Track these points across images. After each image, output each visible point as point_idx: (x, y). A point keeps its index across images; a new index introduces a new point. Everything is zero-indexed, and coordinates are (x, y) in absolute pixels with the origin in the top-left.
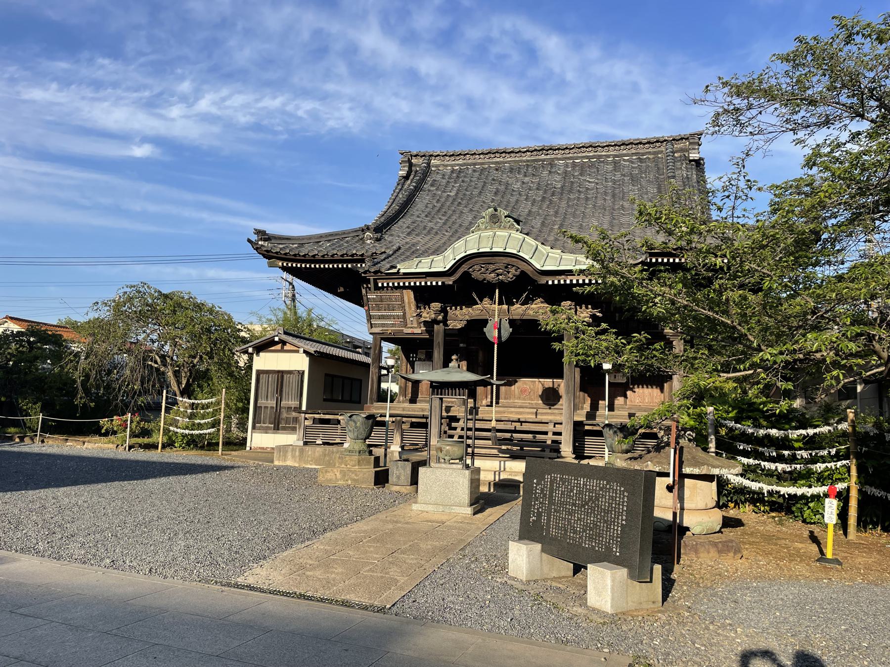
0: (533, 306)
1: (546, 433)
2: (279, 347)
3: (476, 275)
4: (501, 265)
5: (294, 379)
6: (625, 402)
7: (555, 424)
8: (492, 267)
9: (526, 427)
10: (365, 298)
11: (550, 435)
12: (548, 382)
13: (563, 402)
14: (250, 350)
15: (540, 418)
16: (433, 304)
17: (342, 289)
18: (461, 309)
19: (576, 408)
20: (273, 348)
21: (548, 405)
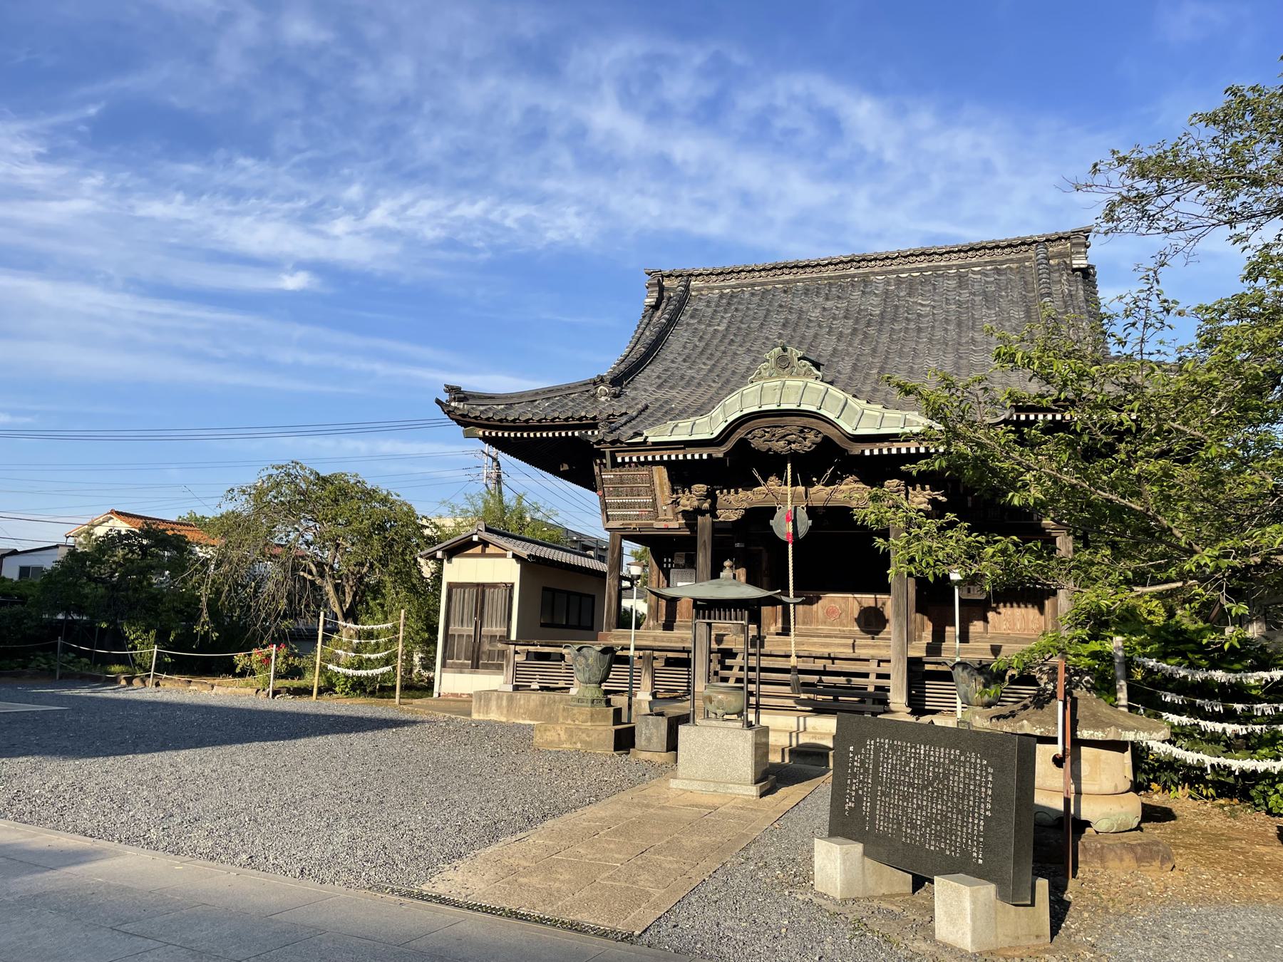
0: (843, 487)
1: (866, 675)
2: (478, 549)
5: (500, 595)
6: (986, 629)
7: (880, 661)
8: (780, 432)
10: (598, 479)
11: (872, 678)
12: (868, 599)
13: (891, 629)
14: (439, 555)
17: (566, 467)
18: (737, 493)
20: (470, 551)
21: (868, 633)
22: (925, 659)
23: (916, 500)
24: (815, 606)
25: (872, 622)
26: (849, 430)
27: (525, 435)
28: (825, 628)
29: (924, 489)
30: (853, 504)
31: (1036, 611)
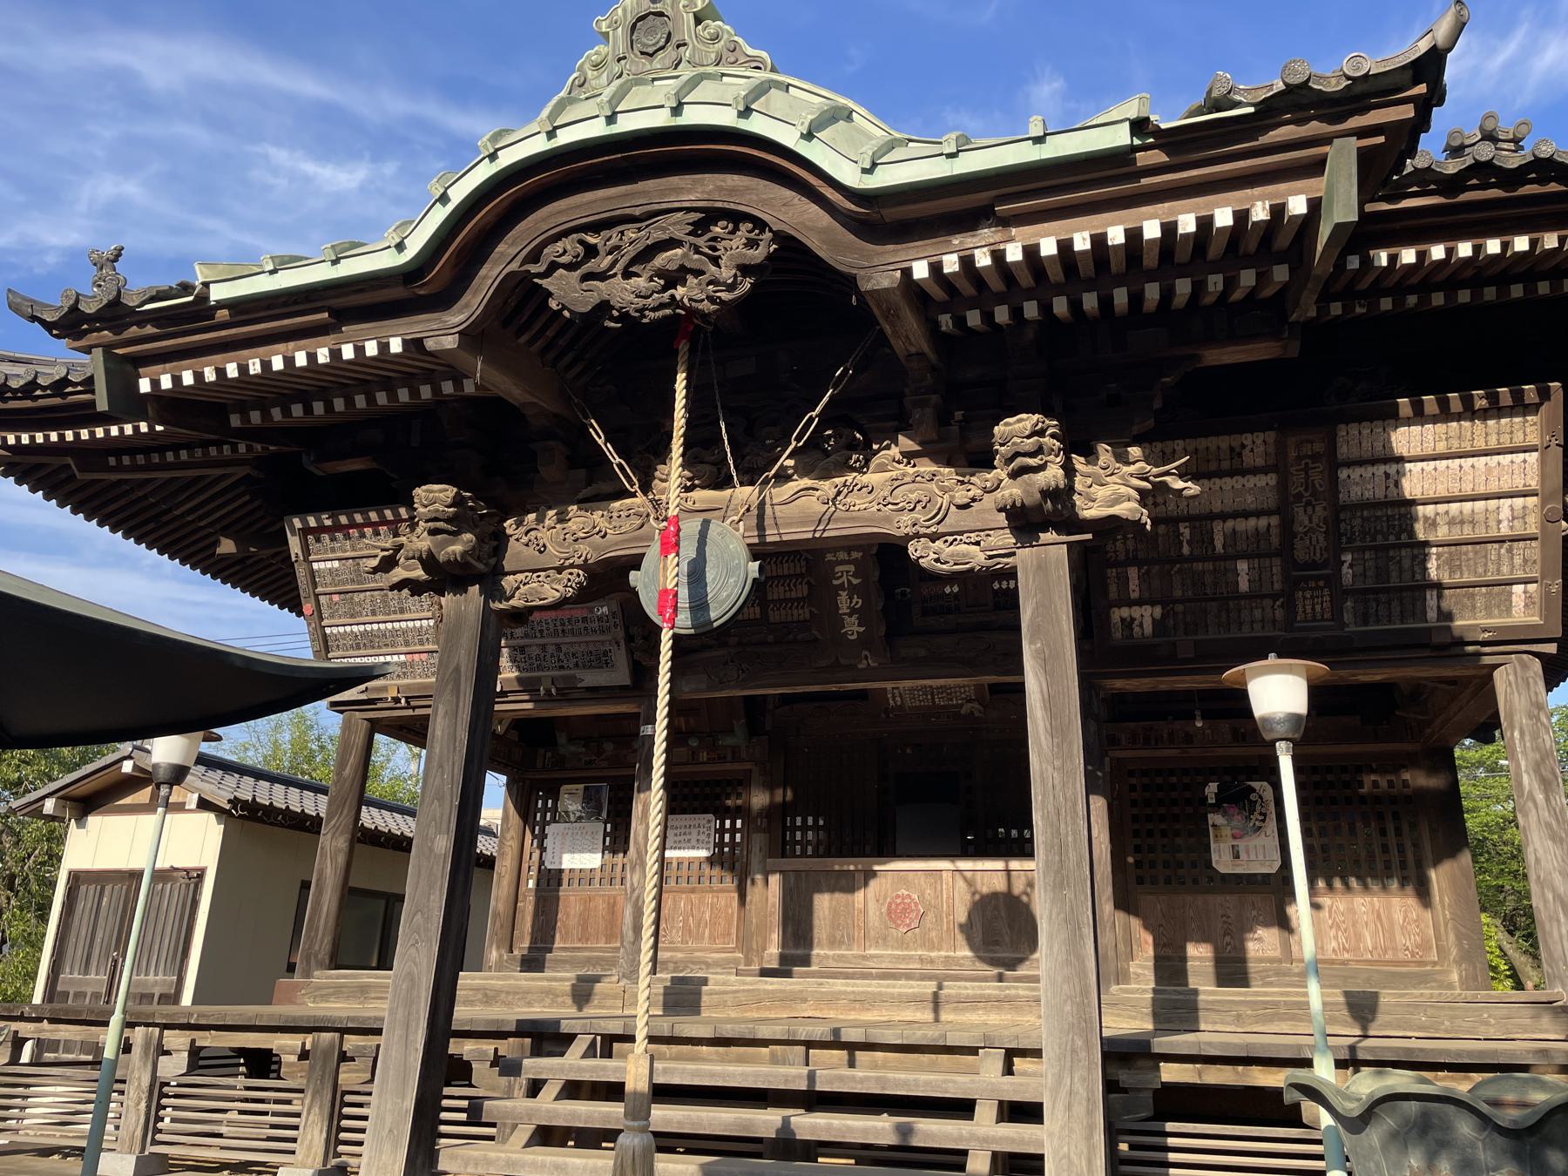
0: (870, 478)
1: (962, 1108)
2: (144, 795)
3: (568, 292)
4: (676, 226)
5: (173, 894)
6: (1287, 947)
7: (1011, 1054)
8: (633, 238)
9: (868, 1076)
10: (301, 572)
11: (986, 1113)
12: (989, 872)
13: (1047, 957)
14: (49, 806)
15: (960, 1024)
16: (420, 492)
17: (227, 546)
18: (562, 519)
19: (1106, 973)
20: (128, 800)
21: (993, 962)
22: (1162, 1044)
23: (1101, 492)
24: (859, 896)
25: (1002, 931)
26: (850, 176)
27: (54, 437)
28: (882, 954)
29: (1123, 459)
30: (901, 525)
31: (1412, 902)
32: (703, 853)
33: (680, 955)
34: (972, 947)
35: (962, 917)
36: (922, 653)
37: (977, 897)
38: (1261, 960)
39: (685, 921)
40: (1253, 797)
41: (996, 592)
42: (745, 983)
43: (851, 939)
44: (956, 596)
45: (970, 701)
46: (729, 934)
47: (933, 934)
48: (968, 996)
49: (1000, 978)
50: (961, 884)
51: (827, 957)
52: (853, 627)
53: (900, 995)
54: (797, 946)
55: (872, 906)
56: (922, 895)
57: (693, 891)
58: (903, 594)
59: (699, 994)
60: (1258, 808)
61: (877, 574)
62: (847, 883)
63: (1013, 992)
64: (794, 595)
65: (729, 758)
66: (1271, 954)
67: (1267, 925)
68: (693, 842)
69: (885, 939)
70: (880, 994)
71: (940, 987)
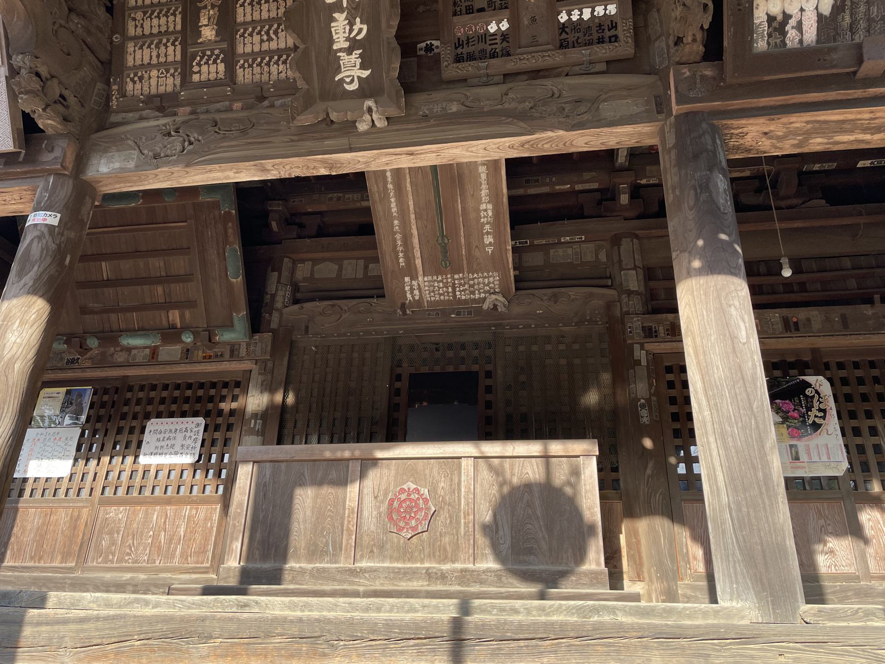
21: (527, 576)
24: (353, 490)
32: (188, 459)
33: (142, 576)
34: (499, 556)
35: (488, 517)
36: (454, 108)
37: (506, 489)
38: (835, 578)
39: (155, 537)
40: (809, 392)
41: (563, 27)
42: (108, 605)
43: (338, 547)
44: (504, 36)
45: (495, 293)
46: (205, 552)
47: (447, 539)
48: (521, 626)
49: (542, 596)
50: (485, 475)
51: (302, 571)
52: (352, 71)
53: (389, 625)
54: (265, 558)
55: (368, 501)
56: (433, 490)
57: (169, 502)
58: (429, 48)
59: (18, 623)
60: (816, 404)
61: (395, 23)
62: (338, 475)
63: (607, 618)
64: (273, 45)
65: (227, 356)
66: (846, 570)
67: (837, 534)
68: (177, 448)
69: (382, 547)
70: (351, 623)
71: (465, 609)
